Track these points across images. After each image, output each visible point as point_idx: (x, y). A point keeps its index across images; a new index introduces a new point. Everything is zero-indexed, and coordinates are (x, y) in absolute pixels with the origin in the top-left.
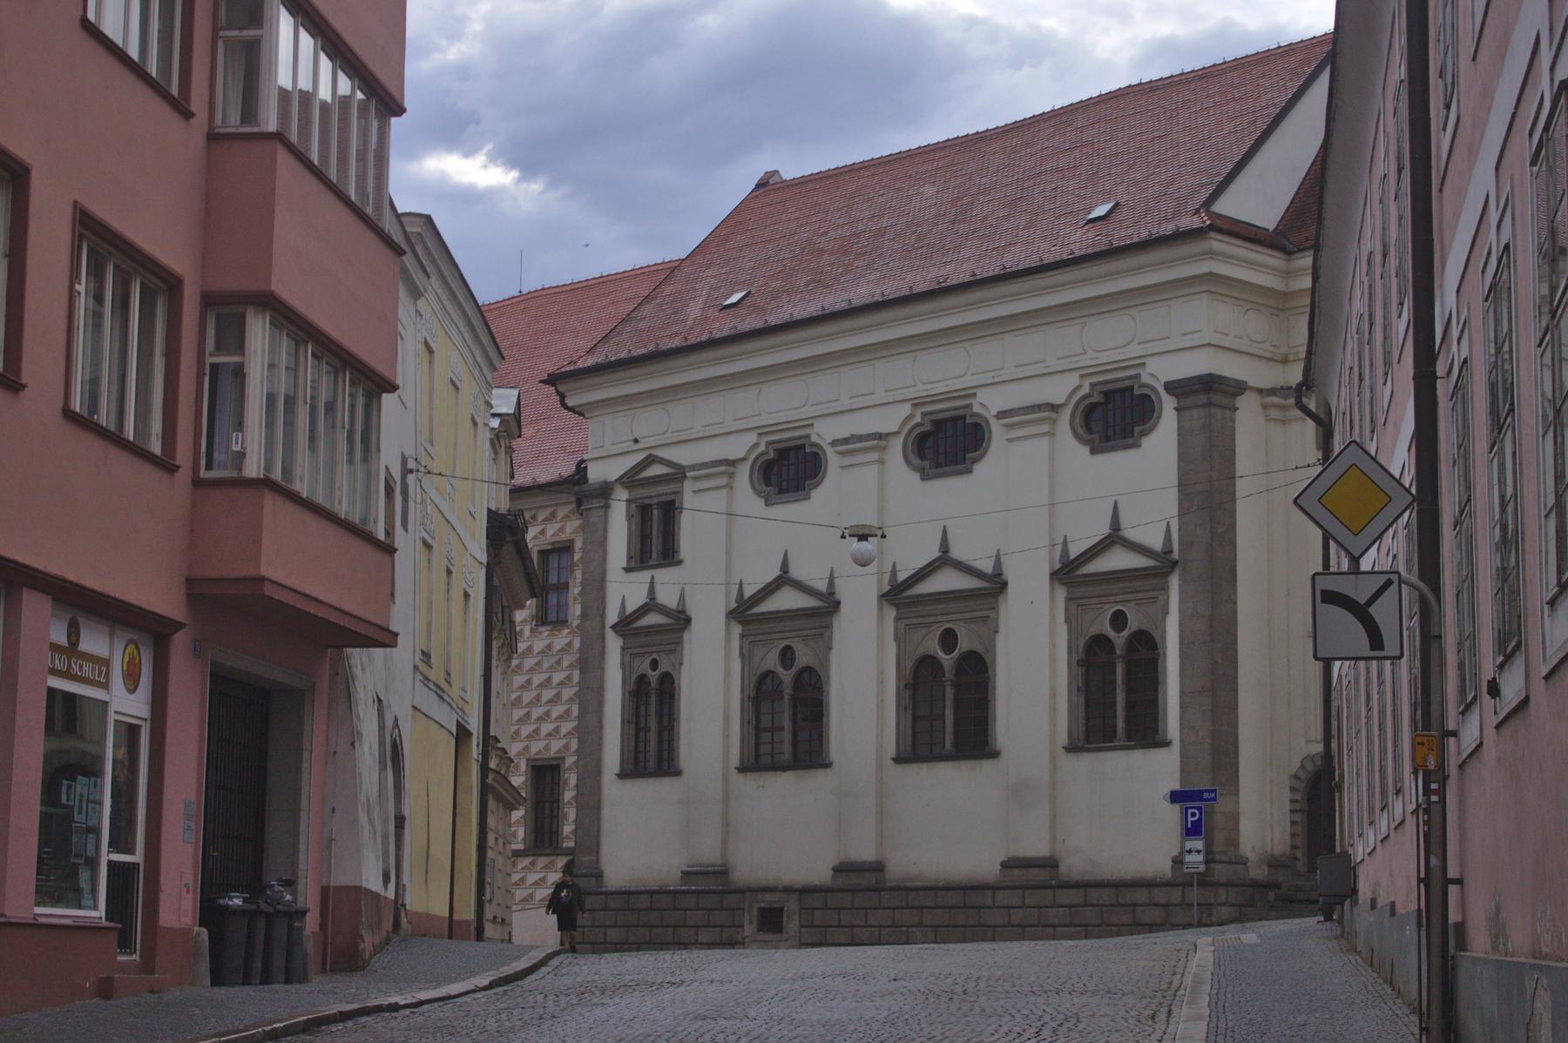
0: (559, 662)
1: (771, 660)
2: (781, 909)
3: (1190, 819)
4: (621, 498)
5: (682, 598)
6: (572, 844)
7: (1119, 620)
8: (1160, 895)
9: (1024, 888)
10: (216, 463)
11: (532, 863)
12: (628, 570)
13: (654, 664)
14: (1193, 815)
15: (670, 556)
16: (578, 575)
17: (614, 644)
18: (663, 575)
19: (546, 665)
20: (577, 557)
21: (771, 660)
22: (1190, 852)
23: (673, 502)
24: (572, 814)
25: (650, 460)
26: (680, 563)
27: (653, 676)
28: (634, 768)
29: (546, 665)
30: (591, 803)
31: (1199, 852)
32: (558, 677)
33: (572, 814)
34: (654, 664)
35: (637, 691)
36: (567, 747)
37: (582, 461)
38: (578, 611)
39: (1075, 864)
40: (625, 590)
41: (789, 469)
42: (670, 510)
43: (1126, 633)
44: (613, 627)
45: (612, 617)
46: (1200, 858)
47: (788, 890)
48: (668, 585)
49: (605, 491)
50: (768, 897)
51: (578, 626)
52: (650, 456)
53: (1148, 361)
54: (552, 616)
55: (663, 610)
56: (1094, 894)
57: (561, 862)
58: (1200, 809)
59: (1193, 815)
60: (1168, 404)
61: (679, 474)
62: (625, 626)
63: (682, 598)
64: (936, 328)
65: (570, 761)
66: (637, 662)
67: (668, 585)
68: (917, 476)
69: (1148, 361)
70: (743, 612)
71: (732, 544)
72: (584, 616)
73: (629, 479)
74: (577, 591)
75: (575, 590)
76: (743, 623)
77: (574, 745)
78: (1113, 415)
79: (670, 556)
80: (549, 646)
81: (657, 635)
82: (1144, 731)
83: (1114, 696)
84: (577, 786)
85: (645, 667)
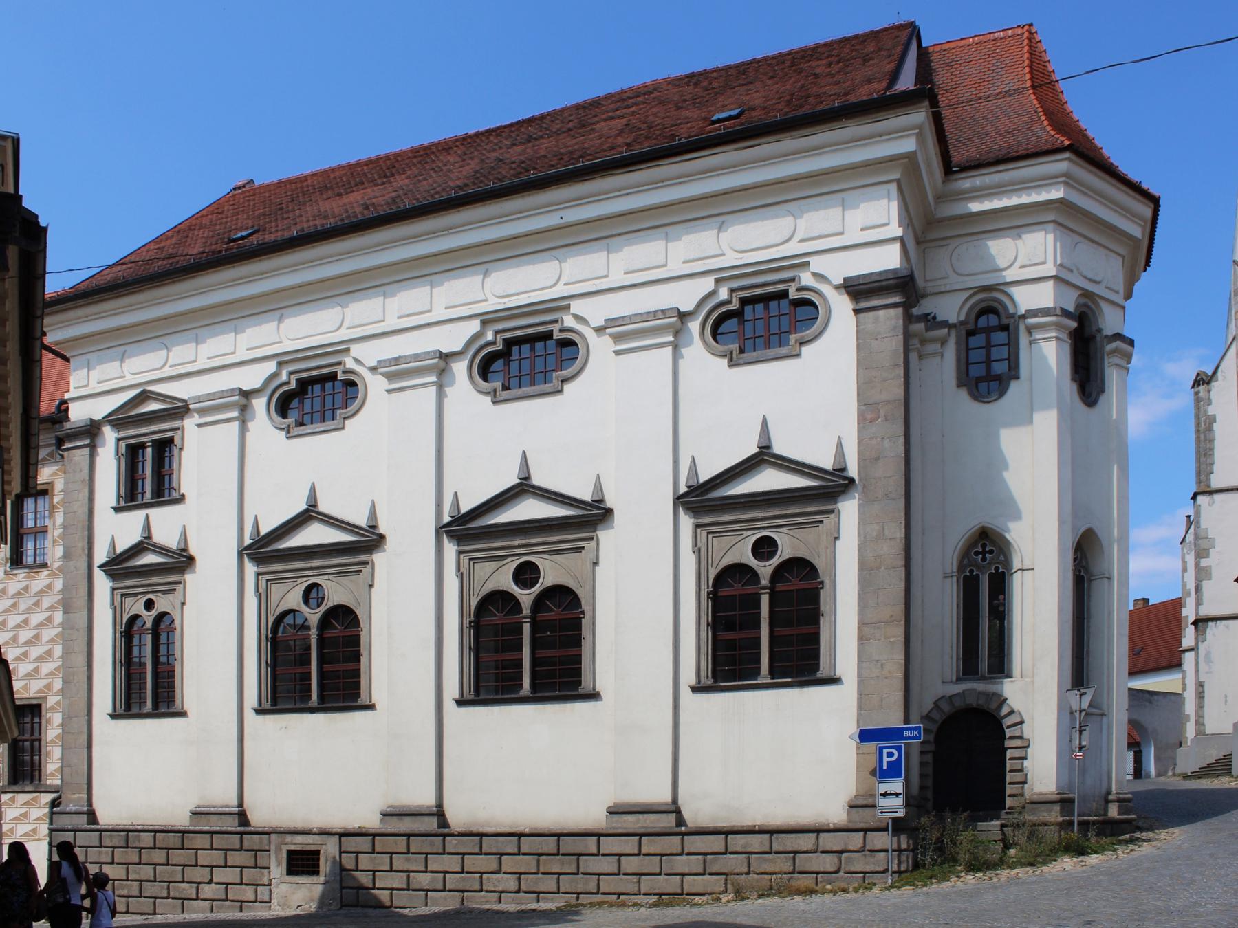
0: (37, 604)
1: (294, 599)
2: (318, 852)
3: (886, 759)
4: (109, 435)
5: (373, 514)
6: (57, 782)
7: (764, 548)
8: (828, 841)
9: (641, 835)
10: (862, 315)
11: (12, 799)
12: (118, 509)
13: (149, 605)
14: (890, 755)
15: (164, 491)
16: (59, 518)
17: (103, 584)
18: (159, 515)
19: (22, 607)
20: (56, 500)
21: (294, 599)
22: (885, 795)
23: (170, 441)
24: (56, 752)
25: (144, 397)
26: (181, 500)
27: (149, 617)
28: (129, 705)
29: (22, 607)
30: (83, 743)
31: (897, 795)
32: (36, 619)
33: (56, 752)
34: (149, 605)
35: (128, 632)
36: (48, 687)
37: (65, 402)
38: (59, 551)
39: (700, 808)
40: (117, 530)
41: (314, 395)
42: (164, 448)
43: (537, 589)
44: (100, 567)
45: (101, 556)
46: (899, 801)
47: (324, 833)
48: (166, 525)
49: (91, 430)
50: (299, 839)
51: (59, 569)
52: (144, 392)
53: (813, 260)
54: (29, 560)
55: (162, 550)
56: (737, 842)
57: (48, 798)
58: (898, 749)
59: (890, 755)
60: (841, 308)
61: (180, 410)
62: (118, 566)
63: (373, 514)
64: (1079, 204)
65: (52, 701)
66: (129, 601)
67: (166, 525)
68: (488, 399)
69: (813, 260)
70: (264, 550)
71: (240, 476)
72: (67, 556)
73: (119, 419)
74: (57, 532)
75: (55, 532)
76: (259, 560)
77: (58, 684)
78: (760, 317)
79: (164, 491)
80: (26, 588)
81: (151, 572)
82: (800, 663)
83: (759, 628)
84: (62, 725)
85: (137, 607)
